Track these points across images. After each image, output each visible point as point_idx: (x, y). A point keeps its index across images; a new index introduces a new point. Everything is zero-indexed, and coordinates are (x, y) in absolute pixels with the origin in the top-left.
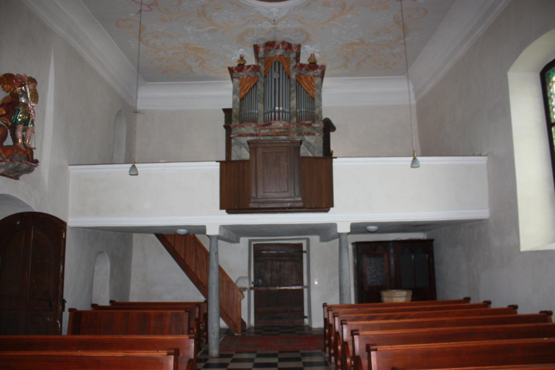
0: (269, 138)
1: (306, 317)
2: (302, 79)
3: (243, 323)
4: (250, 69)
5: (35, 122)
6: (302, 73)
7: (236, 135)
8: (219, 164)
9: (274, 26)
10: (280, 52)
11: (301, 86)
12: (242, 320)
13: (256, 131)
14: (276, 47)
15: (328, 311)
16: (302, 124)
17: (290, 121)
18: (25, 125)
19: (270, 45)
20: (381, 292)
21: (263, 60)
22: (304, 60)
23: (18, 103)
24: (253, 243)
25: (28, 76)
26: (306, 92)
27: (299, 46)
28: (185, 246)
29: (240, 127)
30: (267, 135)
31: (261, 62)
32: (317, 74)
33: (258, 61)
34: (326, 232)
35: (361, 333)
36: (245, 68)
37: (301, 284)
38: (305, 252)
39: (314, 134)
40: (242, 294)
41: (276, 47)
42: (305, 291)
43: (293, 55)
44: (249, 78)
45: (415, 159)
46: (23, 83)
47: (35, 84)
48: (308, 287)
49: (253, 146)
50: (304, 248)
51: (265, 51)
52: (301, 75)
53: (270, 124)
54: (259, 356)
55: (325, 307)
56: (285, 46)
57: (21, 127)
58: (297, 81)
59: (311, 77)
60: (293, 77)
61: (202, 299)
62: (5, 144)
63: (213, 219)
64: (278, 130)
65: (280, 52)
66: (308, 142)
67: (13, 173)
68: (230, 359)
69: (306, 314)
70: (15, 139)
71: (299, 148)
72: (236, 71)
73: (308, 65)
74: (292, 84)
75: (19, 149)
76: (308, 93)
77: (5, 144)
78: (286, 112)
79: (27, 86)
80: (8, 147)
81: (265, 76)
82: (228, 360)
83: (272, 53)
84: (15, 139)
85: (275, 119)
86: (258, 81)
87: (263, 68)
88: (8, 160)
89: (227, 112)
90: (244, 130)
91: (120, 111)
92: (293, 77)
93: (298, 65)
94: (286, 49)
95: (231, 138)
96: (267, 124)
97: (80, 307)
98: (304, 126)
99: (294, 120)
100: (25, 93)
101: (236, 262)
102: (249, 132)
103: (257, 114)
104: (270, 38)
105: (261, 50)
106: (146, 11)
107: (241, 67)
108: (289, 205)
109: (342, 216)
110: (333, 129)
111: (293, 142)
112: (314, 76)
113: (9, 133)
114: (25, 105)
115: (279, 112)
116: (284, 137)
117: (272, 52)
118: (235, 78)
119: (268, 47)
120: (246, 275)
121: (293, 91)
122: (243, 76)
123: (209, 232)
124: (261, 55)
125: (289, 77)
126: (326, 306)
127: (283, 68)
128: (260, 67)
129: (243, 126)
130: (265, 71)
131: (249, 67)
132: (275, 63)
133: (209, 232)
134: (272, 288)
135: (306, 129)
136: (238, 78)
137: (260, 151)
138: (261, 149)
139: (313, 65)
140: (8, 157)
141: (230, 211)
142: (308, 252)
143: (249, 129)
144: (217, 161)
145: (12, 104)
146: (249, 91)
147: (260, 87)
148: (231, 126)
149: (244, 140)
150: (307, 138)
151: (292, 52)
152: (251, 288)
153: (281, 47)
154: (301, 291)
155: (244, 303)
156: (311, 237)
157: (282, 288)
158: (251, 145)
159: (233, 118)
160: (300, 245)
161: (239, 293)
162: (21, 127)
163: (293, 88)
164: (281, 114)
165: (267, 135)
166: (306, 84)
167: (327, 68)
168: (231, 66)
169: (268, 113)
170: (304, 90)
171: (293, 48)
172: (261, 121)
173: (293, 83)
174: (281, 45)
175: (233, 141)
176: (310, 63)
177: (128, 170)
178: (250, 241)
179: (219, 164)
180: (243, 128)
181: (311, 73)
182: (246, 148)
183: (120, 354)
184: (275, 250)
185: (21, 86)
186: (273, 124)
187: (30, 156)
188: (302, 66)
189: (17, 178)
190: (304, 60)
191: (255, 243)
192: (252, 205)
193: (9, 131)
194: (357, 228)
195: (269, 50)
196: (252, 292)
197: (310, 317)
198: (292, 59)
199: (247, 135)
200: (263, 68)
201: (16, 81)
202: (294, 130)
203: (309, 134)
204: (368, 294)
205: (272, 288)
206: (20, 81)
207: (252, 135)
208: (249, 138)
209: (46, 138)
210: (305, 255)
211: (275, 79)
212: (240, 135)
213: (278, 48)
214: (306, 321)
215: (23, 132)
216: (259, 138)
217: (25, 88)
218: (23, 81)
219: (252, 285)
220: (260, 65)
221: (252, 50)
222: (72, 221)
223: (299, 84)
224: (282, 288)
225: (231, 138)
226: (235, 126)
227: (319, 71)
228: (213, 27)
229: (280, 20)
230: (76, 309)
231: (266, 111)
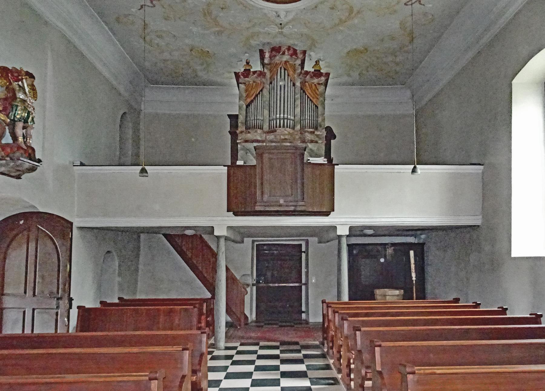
0: (274, 144)
1: (304, 312)
2: (305, 86)
3: (246, 318)
4: (256, 75)
5: (35, 119)
6: (307, 80)
7: (242, 140)
8: (226, 168)
9: (280, 30)
10: (286, 58)
11: (306, 94)
12: (245, 315)
13: (261, 137)
14: (281, 53)
15: (328, 307)
16: (305, 132)
17: (293, 128)
18: (24, 123)
19: (276, 50)
20: (375, 290)
21: (269, 67)
22: (309, 67)
23: (14, 97)
24: (256, 243)
25: (25, 70)
26: (310, 100)
27: (304, 52)
28: (194, 248)
29: (246, 133)
30: (272, 142)
31: (267, 68)
32: (321, 82)
33: (263, 68)
34: (325, 234)
35: (363, 329)
36: (251, 73)
37: (300, 282)
38: (304, 252)
39: (317, 142)
40: (246, 290)
41: (281, 53)
42: (303, 287)
43: (299, 62)
44: (254, 84)
45: (415, 167)
46: (20, 77)
47: (32, 79)
48: (306, 284)
49: (260, 153)
50: (303, 249)
51: (270, 57)
52: (306, 82)
53: (275, 131)
54: (262, 348)
55: (324, 304)
56: (291, 52)
57: (20, 125)
58: (301, 89)
59: (315, 85)
60: (298, 84)
61: (209, 295)
62: (4, 141)
63: (223, 222)
64: (282, 137)
65: (286, 58)
66: (311, 150)
67: (15, 172)
68: (235, 351)
69: (303, 309)
70: (15, 137)
71: (303, 154)
72: (242, 77)
73: (313, 73)
74: (297, 91)
75: (19, 148)
76: (312, 101)
77: (4, 141)
78: (290, 119)
79: (24, 80)
80: (8, 145)
81: (271, 83)
82: (233, 352)
83: (277, 59)
84: (15, 137)
85: (280, 127)
86: (263, 88)
87: (268, 75)
88: (8, 159)
89: (234, 118)
90: (249, 136)
91: (125, 113)
92: (298, 84)
93: (303, 72)
94: (291, 56)
95: (237, 144)
96: (272, 131)
97: (89, 304)
98: (307, 134)
99: (298, 127)
100: (22, 88)
101: (238, 263)
102: (255, 138)
103: (263, 120)
104: (277, 41)
105: (267, 55)
106: (148, 6)
107: (247, 73)
108: (292, 208)
109: (343, 219)
110: (334, 137)
111: (296, 148)
112: (319, 84)
113: (7, 131)
114: (24, 101)
115: (284, 119)
116: (288, 144)
117: (277, 58)
118: (241, 83)
119: (274, 53)
120: (250, 273)
121: (297, 99)
122: (249, 82)
123: (216, 233)
124: (266, 61)
125: (294, 85)
126: (325, 302)
127: (288, 75)
128: (265, 73)
129: (249, 133)
130: (270, 78)
131: (255, 72)
132: (281, 68)
133: (216, 233)
134: (271, 285)
135: (309, 137)
136: (245, 83)
137: (266, 156)
138: (267, 155)
139: (317, 73)
140: (8, 156)
141: (236, 214)
142: (307, 252)
143: (258, 135)
144: (224, 166)
145: (10, 100)
146: (255, 98)
147: (265, 92)
148: (238, 132)
149: (251, 146)
150: (310, 146)
151: (298, 58)
152: (253, 285)
153: (286, 53)
154: (300, 287)
155: (247, 298)
156: (310, 239)
157: (280, 285)
158: (257, 151)
159: (239, 124)
160: (300, 245)
161: (243, 290)
162: (20, 125)
163: (298, 96)
164: (286, 121)
165: (272, 142)
166: (309, 91)
167: (330, 76)
168: (237, 71)
169: (273, 120)
170: (308, 97)
171: (299, 55)
172: (266, 127)
173: (298, 90)
174: (286, 51)
175: (239, 146)
176: (315, 70)
177: (139, 171)
178: (253, 242)
179: (226, 168)
180: (249, 134)
181: (316, 81)
182: (252, 155)
183: (135, 350)
184: (276, 250)
185: (18, 80)
186: (278, 131)
187: (32, 155)
188: (307, 73)
189: (18, 177)
190: (309, 67)
191: (258, 243)
192: (258, 208)
193: (7, 127)
194: (354, 231)
195: (275, 56)
196: (255, 288)
197: (307, 312)
198: (297, 66)
199: (253, 141)
200: (268, 75)
201: (12, 75)
202: (297, 137)
203: (312, 141)
204: (361, 291)
205: (271, 285)
206: (16, 75)
207: (258, 141)
208: (255, 144)
209: (50, 133)
210: (304, 255)
211: (281, 86)
212: (246, 141)
213: (284, 53)
214: (304, 316)
215: (23, 129)
216: (265, 144)
217: (22, 83)
218: (19, 76)
219: (255, 282)
220: (266, 71)
221: (258, 55)
222: (77, 223)
223: (304, 92)
224: (280, 285)
225: (237, 144)
226: (242, 132)
227: (323, 79)
228: (217, 29)
229: (287, 23)
230: (84, 307)
231: (271, 118)
